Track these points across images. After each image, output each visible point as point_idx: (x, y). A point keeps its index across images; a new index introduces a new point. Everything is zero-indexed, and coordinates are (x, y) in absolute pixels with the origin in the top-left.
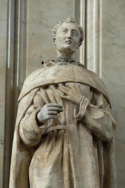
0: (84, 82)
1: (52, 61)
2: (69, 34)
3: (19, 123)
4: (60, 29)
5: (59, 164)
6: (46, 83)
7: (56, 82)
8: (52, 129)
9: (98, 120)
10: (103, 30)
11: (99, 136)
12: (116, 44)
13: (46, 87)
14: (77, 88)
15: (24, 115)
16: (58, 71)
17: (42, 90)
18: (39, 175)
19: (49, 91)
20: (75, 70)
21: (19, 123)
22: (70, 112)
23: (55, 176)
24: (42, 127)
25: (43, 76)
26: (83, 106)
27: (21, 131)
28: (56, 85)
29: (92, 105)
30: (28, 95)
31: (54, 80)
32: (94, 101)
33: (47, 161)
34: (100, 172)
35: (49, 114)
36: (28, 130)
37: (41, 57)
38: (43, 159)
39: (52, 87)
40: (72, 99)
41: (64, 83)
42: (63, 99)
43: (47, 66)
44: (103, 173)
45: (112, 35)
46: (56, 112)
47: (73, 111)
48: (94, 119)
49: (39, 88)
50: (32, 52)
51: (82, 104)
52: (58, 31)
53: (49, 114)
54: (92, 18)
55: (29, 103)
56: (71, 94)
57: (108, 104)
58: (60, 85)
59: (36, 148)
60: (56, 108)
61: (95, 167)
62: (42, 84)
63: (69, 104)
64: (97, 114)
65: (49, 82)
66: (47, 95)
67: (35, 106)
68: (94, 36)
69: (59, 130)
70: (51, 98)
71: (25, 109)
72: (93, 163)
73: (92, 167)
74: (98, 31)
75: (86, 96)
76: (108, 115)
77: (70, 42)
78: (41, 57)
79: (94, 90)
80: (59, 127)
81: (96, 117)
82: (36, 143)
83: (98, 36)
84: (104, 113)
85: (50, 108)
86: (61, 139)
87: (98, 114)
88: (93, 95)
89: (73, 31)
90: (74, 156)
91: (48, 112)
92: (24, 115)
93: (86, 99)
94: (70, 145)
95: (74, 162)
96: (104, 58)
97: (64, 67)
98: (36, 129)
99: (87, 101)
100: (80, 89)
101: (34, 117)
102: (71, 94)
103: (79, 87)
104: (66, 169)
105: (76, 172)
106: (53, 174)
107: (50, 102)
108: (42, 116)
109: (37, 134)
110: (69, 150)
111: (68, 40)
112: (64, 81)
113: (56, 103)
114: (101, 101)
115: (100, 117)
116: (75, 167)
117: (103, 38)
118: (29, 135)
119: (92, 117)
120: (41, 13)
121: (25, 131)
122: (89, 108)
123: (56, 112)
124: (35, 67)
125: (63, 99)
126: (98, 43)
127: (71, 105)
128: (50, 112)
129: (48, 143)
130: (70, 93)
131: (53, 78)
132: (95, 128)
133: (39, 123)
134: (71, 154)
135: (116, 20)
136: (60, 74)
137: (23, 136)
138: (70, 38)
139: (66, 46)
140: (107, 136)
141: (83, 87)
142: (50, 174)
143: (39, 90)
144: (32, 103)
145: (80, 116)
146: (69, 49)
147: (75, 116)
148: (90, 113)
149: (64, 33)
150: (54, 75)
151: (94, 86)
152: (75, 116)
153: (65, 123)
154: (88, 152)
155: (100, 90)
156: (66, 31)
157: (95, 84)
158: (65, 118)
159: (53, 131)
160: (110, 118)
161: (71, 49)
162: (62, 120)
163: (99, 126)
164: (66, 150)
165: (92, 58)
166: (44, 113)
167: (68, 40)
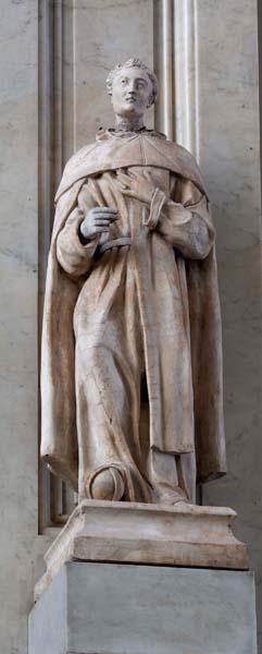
0: (159, 163)
1: (110, 130)
2: (130, 87)
3: (56, 240)
4: (117, 78)
5: (117, 307)
6: (97, 170)
7: (113, 167)
8: (109, 244)
9: (181, 227)
10: (200, 67)
11: (185, 252)
12: (222, 89)
13: (98, 176)
14: (147, 175)
15: (63, 226)
16: (117, 148)
17: (90, 181)
18: (85, 323)
19: (103, 183)
20: (145, 146)
21: (56, 240)
22: (137, 215)
23: (112, 326)
24: (88, 245)
25: (93, 159)
26: (156, 206)
27: (59, 253)
28: (113, 173)
29: (172, 203)
30: (69, 192)
31: (110, 165)
32: (176, 196)
33: (99, 301)
34: (191, 309)
35: (97, 225)
36: (68, 250)
37: (98, 120)
38: (94, 297)
39: (107, 175)
40: (138, 195)
41: (125, 169)
42: (124, 195)
43: (101, 139)
44: (198, 310)
45: (216, 75)
46: (106, 222)
47: (141, 214)
48: (175, 226)
49: (86, 179)
50: (79, 114)
51: (155, 203)
52: (115, 82)
53: (97, 225)
54: (183, 49)
55: (72, 203)
56: (136, 187)
57: (202, 198)
58: (118, 173)
59: (85, 277)
60: (107, 216)
61: (179, 304)
62: (91, 172)
63: (134, 203)
64: (181, 217)
65: (102, 169)
66: (98, 187)
67: (81, 208)
68: (187, 78)
69: (120, 247)
70: (107, 195)
71: (64, 215)
72: (175, 298)
73: (174, 306)
74: (192, 69)
75: (162, 189)
76: (199, 216)
77: (133, 100)
78: (98, 120)
79: (177, 177)
80: (120, 241)
81: (178, 223)
82: (83, 272)
83: (192, 79)
84: (193, 213)
85: (98, 216)
86: (123, 261)
87: (182, 217)
88: (176, 184)
89: (137, 81)
90: (142, 290)
91: (94, 222)
92: (63, 226)
93: (162, 193)
94: (136, 272)
95: (143, 299)
96: (204, 113)
97: (125, 140)
98: (80, 249)
99: (164, 196)
100: (152, 179)
101: (74, 231)
102: (136, 187)
103: (150, 173)
104: (129, 312)
105: (145, 317)
106: (107, 323)
107: (106, 205)
108: (86, 229)
109: (82, 258)
110: (135, 280)
111: (130, 96)
112: (126, 165)
113: (106, 205)
114: (188, 193)
115: (186, 221)
116: (144, 307)
117: (201, 81)
118: (71, 259)
119: (170, 222)
120: (97, 47)
121: (64, 253)
122: (166, 209)
123: (106, 222)
124: (86, 138)
125: (124, 195)
126: (192, 90)
127: (139, 204)
128: (99, 222)
129: (102, 271)
130: (134, 184)
131: (108, 161)
132: (177, 239)
133: (83, 240)
134: (138, 287)
135: (222, 48)
136: (119, 154)
137: (61, 260)
138: (133, 93)
139: (127, 106)
140: (199, 251)
141: (158, 173)
142: (103, 323)
143: (86, 182)
144: (76, 204)
145: (151, 222)
146: (133, 111)
147: (144, 223)
148: (168, 217)
149: (124, 86)
150: (111, 155)
151: (177, 169)
152: (144, 223)
153: (129, 235)
154: (167, 283)
155: (186, 174)
156: (126, 81)
157: (178, 166)
158: (129, 227)
159: (111, 249)
160: (62, 381)
161: (137, 111)
162: (124, 230)
163: (184, 236)
164: (129, 281)
165: (183, 114)
166: (90, 227)
167: (130, 96)
